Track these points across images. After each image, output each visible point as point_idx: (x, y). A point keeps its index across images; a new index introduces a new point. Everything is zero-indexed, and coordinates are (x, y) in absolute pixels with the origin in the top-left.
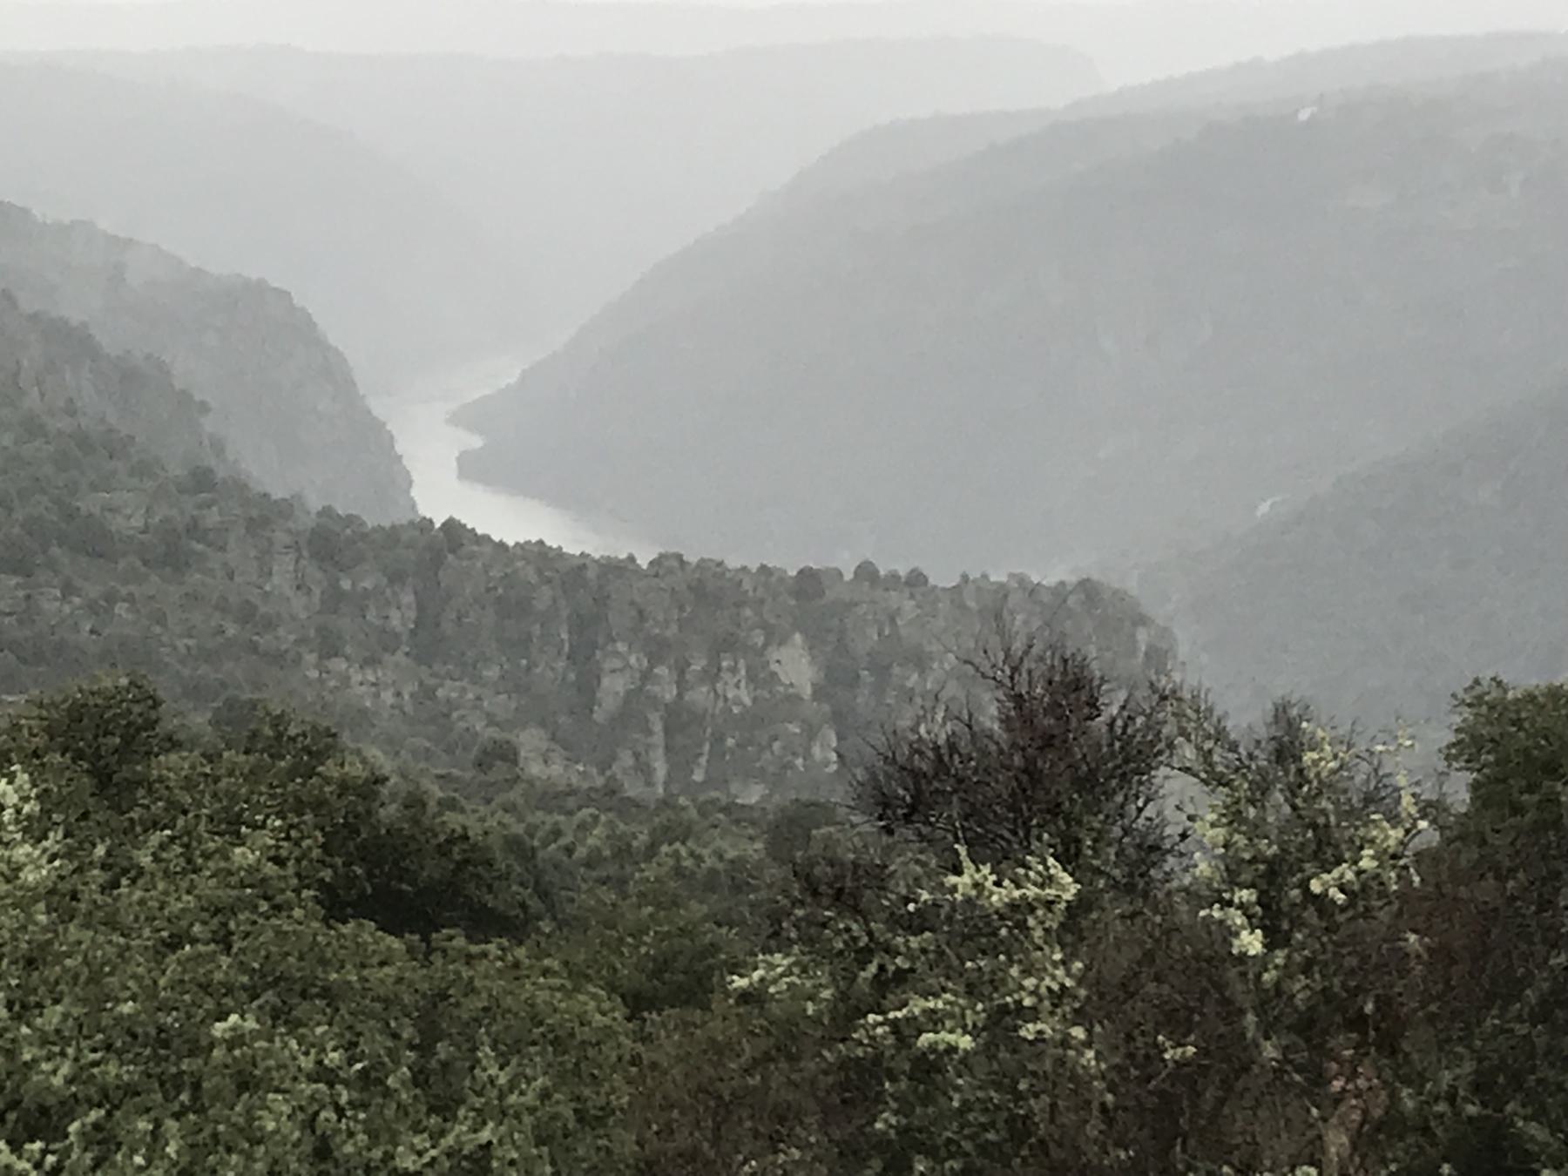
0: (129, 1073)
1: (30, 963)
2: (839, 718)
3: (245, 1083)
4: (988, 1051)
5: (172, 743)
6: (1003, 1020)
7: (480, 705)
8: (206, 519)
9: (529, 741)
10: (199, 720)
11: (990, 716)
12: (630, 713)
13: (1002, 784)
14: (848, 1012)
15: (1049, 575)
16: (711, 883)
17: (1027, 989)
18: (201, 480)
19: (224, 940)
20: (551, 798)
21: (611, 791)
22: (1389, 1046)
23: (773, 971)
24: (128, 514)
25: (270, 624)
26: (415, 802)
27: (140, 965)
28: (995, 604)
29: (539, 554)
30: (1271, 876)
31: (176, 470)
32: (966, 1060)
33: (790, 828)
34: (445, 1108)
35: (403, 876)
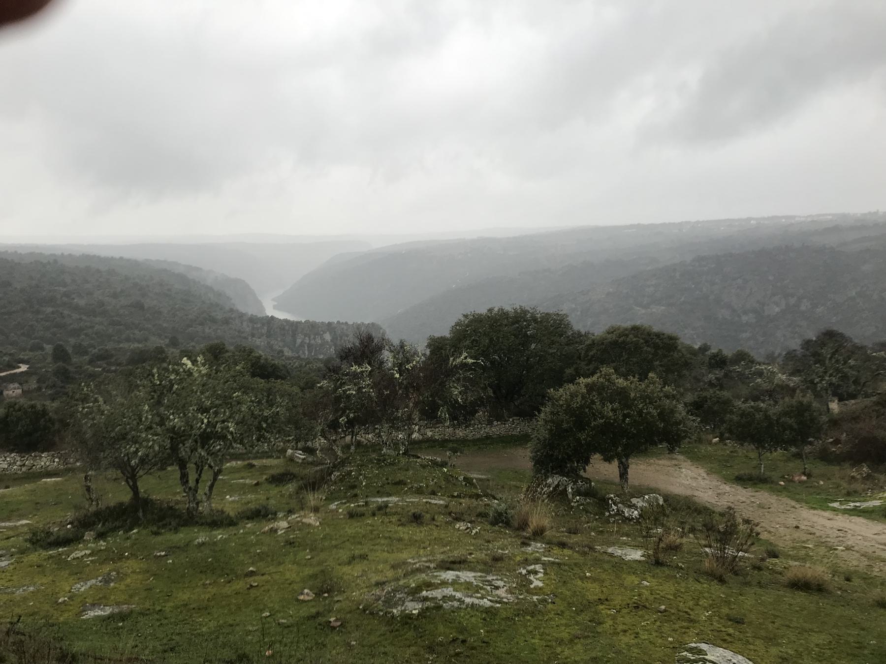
0: (220, 402)
1: (203, 386)
3: (239, 403)
4: (358, 393)
5: (227, 351)
6: (360, 389)
7: (277, 345)
8: (232, 317)
9: (286, 349)
10: (232, 348)
13: (359, 353)
14: (336, 389)
15: (367, 322)
17: (363, 384)
18: (231, 310)
19: (235, 381)
20: (288, 358)
21: (299, 357)
23: (324, 383)
24: (219, 316)
26: (266, 359)
27: (221, 385)
28: (358, 327)
29: (286, 321)
30: (400, 365)
31: (227, 308)
33: (327, 362)
34: (272, 406)
35: (264, 370)
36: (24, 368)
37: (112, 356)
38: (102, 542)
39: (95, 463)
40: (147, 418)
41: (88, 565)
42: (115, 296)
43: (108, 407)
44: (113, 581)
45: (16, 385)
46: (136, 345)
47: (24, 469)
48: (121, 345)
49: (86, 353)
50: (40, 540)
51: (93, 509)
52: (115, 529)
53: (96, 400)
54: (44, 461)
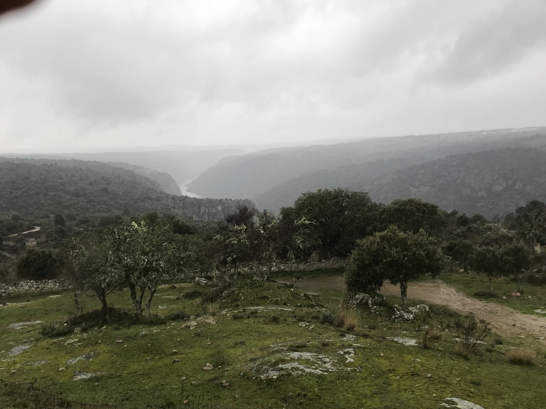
2: (224, 213)
4: (238, 243)
6: (239, 240)
7: (189, 213)
8: (161, 197)
9: (194, 216)
11: (238, 212)
12: (204, 213)
13: (239, 218)
14: (225, 240)
16: (212, 229)
18: (161, 192)
20: (196, 221)
22: (275, 240)
23: (218, 237)
25: (168, 206)
26: (183, 222)
29: (194, 198)
31: (158, 191)
32: (236, 244)
33: (219, 223)
34: (186, 251)
35: (181, 229)
36: (38, 229)
37: (90, 221)
38: (85, 334)
39: (80, 286)
40: (111, 259)
41: (77, 348)
42: (91, 184)
43: (88, 252)
44: (92, 357)
45: (33, 239)
46: (104, 214)
47: (38, 290)
48: (95, 215)
49: (74, 219)
50: (49, 333)
51: (79, 314)
52: (92, 326)
53: (81, 248)
54: (50, 285)
